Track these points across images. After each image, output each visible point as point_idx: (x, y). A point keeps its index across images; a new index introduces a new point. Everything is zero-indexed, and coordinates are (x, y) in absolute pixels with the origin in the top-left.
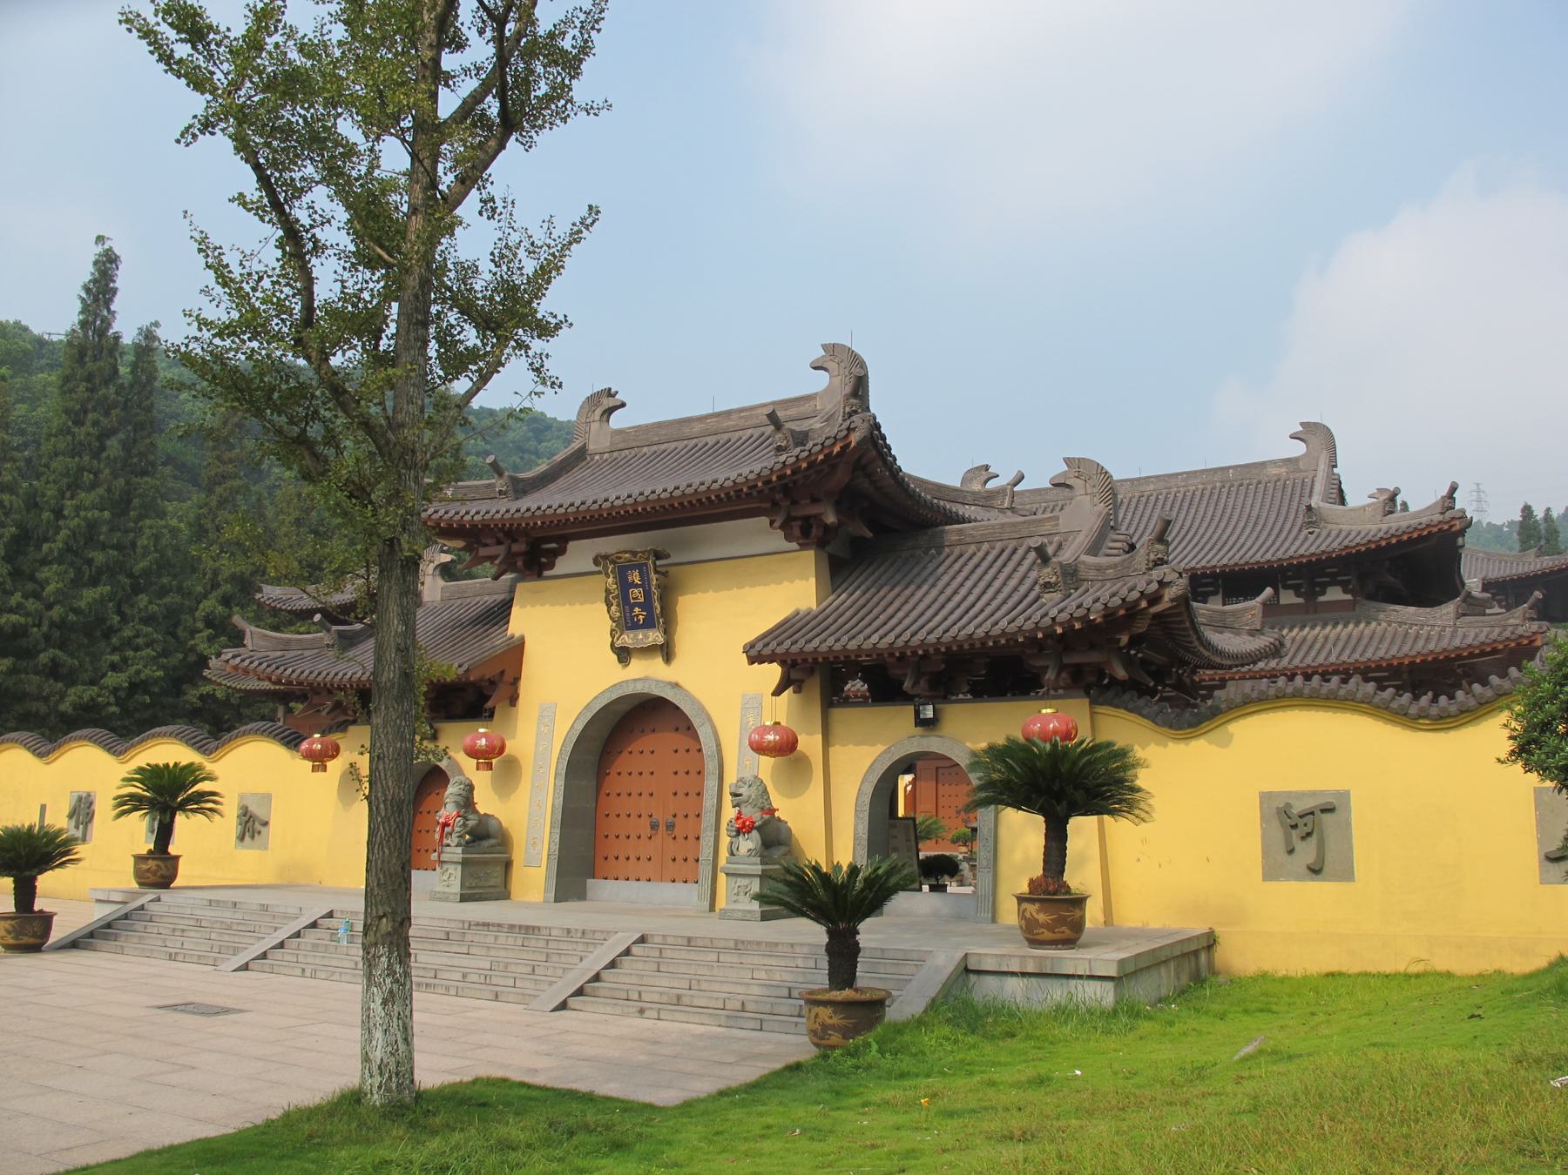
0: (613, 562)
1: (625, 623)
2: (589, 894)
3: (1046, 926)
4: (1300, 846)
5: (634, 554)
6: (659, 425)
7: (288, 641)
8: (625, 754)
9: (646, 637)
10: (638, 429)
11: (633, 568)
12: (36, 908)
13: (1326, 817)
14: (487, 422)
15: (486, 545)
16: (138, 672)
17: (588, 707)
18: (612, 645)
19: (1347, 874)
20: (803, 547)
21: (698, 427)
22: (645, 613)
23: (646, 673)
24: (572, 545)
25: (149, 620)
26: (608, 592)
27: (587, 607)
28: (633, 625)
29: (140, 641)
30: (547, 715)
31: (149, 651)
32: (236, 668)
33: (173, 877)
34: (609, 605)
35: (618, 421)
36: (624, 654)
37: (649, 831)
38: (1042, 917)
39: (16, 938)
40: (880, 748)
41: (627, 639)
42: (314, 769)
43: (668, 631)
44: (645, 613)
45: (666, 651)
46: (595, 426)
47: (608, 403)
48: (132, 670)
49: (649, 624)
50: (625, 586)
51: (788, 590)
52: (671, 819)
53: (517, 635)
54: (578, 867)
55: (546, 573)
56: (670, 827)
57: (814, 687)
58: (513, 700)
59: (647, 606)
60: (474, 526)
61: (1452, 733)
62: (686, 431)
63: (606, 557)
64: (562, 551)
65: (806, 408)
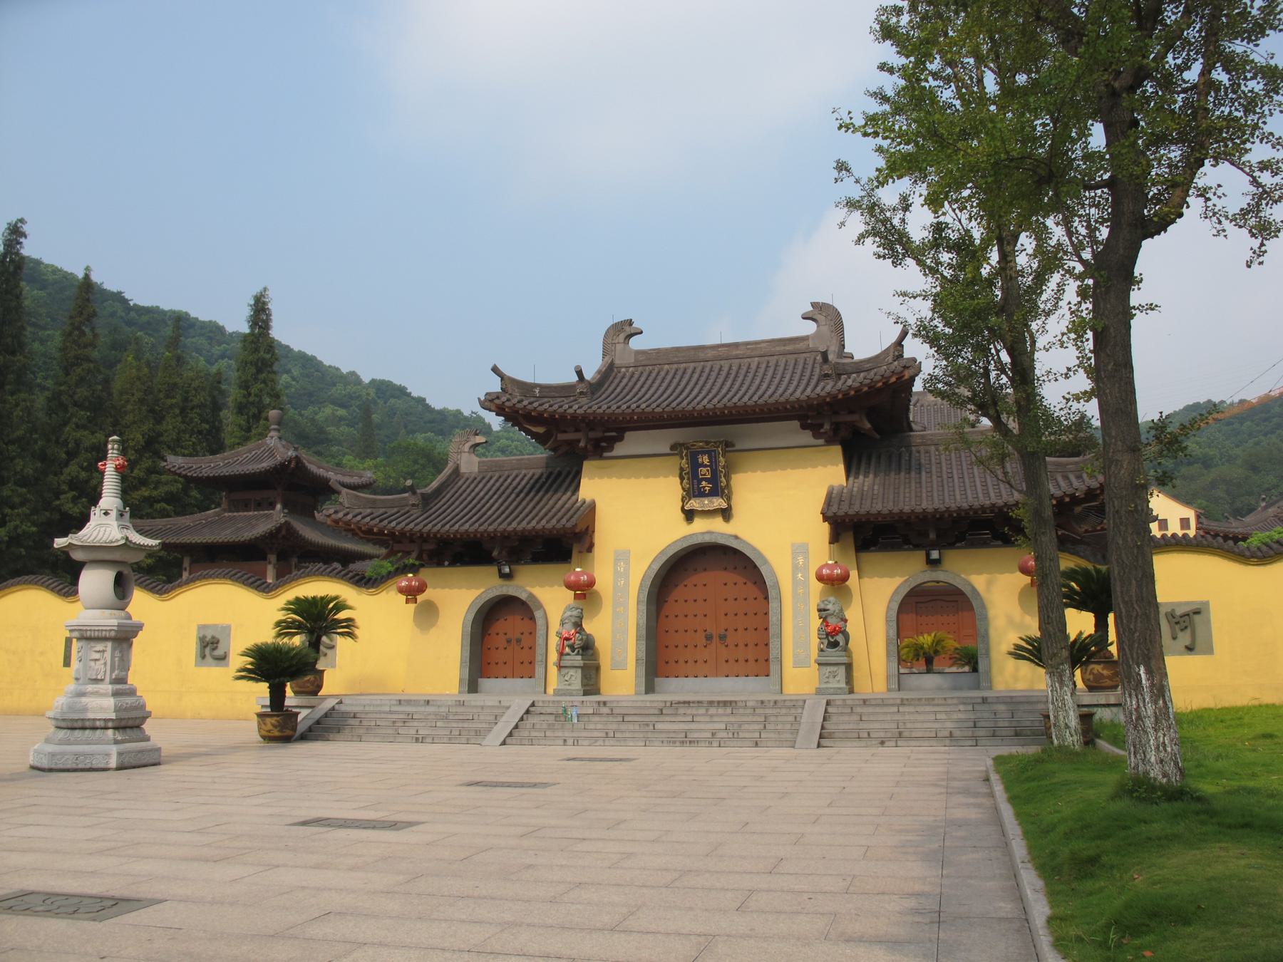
0: (687, 448)
1: (693, 490)
2: (657, 688)
3: (1108, 677)
4: (1180, 635)
5: (707, 443)
6: (677, 349)
7: (374, 501)
8: (681, 587)
9: (711, 502)
10: (658, 351)
11: (703, 453)
12: (1038, 634)
13: (1197, 618)
14: (145, 318)
15: (565, 432)
16: (16, 527)
17: (662, 552)
18: (683, 509)
19: (1209, 650)
20: (829, 442)
21: (711, 354)
22: (706, 483)
23: (704, 529)
24: (628, 435)
25: (24, 482)
26: (682, 469)
27: (651, 480)
28: (701, 494)
29: (17, 500)
30: (622, 557)
31: (25, 510)
32: (336, 522)
33: (320, 687)
34: (682, 479)
35: (636, 344)
36: (689, 515)
37: (704, 642)
38: (1105, 672)
39: (281, 731)
40: (898, 581)
41: (694, 504)
42: (407, 601)
43: (729, 499)
44: (706, 483)
45: (726, 514)
46: (619, 347)
47: (628, 330)
48: (11, 525)
49: (715, 492)
50: (695, 465)
51: (824, 475)
52: (723, 632)
53: (588, 500)
54: (657, 664)
55: (606, 454)
56: (722, 638)
57: (849, 540)
58: (590, 548)
59: (714, 480)
60: (552, 416)
61: (1269, 567)
62: (702, 355)
63: (682, 445)
64: (620, 438)
65: (801, 346)
